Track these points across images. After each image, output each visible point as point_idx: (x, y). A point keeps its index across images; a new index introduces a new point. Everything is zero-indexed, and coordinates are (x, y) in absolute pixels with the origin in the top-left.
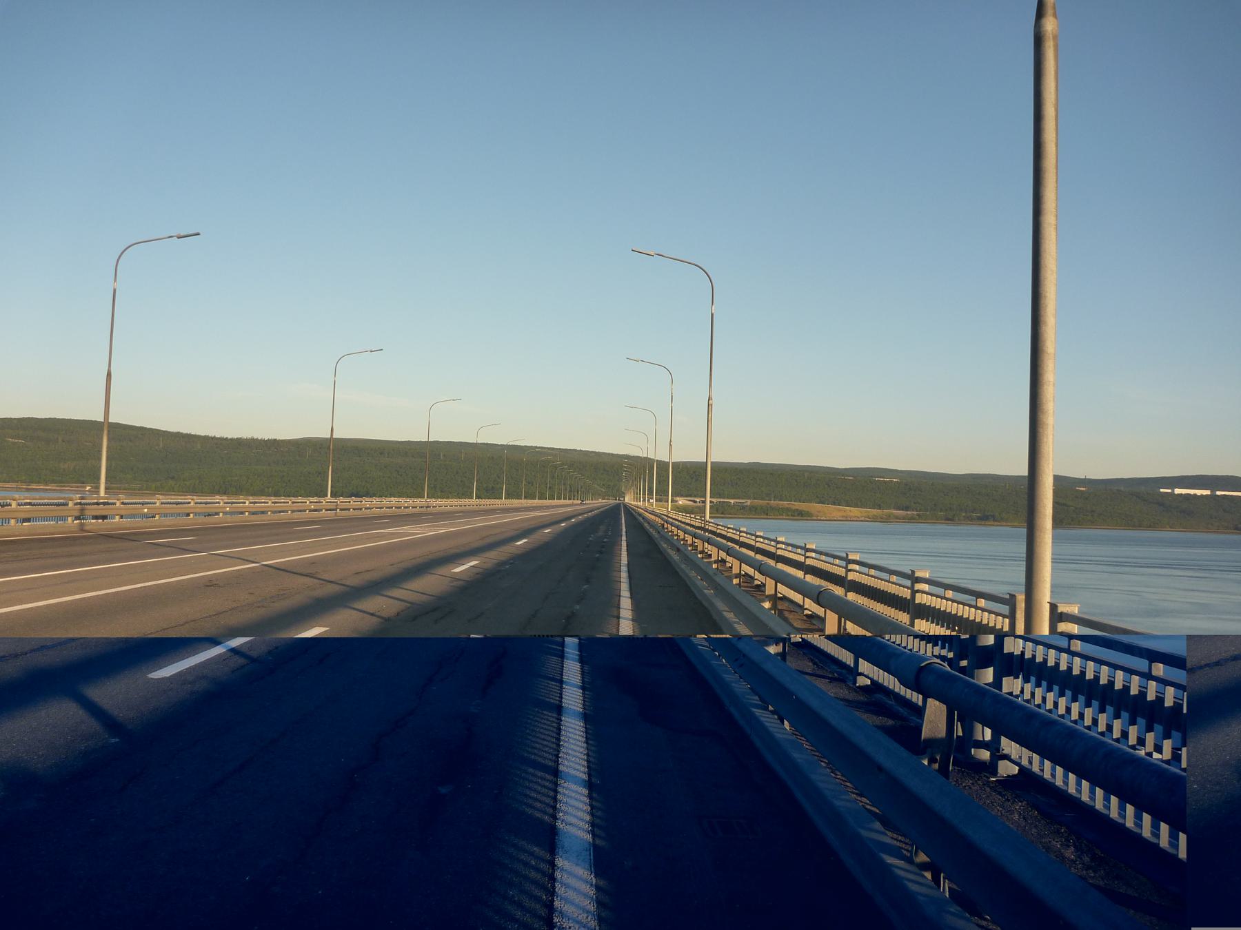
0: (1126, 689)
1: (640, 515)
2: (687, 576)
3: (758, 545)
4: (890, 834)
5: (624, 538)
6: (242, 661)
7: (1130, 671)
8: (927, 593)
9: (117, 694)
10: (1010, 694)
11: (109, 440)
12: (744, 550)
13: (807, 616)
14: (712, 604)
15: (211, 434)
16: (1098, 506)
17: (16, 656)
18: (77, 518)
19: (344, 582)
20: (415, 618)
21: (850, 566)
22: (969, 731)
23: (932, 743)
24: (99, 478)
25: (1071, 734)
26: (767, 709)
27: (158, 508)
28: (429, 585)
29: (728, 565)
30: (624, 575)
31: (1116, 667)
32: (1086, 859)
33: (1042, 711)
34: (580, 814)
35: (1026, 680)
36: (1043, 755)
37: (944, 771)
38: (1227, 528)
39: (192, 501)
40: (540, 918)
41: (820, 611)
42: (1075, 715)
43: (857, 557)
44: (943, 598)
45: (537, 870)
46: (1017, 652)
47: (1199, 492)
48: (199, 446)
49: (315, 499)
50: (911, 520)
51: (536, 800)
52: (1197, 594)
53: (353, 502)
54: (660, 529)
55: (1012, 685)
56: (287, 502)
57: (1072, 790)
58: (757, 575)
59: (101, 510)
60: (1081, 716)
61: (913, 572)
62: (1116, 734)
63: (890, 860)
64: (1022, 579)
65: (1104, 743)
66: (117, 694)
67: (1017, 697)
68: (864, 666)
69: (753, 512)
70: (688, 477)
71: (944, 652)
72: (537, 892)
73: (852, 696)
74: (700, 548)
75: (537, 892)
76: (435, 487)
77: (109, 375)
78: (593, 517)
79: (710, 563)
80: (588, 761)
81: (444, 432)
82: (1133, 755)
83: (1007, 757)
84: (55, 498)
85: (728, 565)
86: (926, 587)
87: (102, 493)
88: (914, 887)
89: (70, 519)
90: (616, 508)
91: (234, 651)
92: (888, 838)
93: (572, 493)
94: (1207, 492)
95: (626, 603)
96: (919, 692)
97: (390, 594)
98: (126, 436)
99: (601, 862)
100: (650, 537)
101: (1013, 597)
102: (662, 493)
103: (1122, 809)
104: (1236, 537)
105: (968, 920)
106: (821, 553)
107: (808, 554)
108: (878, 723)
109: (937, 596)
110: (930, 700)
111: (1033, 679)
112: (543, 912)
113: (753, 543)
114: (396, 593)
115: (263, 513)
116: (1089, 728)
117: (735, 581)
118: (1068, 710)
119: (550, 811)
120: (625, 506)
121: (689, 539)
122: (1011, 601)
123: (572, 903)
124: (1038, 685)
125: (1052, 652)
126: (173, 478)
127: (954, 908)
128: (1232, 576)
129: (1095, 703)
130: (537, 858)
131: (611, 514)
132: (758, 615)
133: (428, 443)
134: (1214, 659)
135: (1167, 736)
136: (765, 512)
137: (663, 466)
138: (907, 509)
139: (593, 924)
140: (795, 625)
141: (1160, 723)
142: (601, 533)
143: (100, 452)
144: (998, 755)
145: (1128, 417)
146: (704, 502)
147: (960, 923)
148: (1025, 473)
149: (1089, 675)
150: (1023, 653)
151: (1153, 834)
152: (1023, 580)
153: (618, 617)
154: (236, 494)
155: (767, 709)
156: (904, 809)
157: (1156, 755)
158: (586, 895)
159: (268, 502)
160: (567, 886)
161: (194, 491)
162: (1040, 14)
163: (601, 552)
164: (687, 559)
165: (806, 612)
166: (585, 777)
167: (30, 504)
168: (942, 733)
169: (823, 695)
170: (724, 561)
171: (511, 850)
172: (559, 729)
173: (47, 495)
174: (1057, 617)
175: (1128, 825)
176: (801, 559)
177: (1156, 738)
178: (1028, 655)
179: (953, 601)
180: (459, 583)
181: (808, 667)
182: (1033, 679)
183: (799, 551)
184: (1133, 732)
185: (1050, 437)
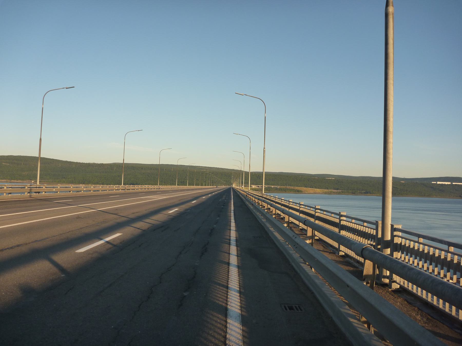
0: (440, 256)
1: (238, 192)
2: (256, 214)
3: (282, 203)
4: (351, 310)
5: (232, 200)
6: (110, 246)
7: (441, 250)
8: (345, 221)
9: (64, 258)
10: (397, 258)
11: (40, 164)
12: (277, 205)
13: (300, 229)
14: (265, 225)
15: (79, 162)
16: (409, 188)
17: (26, 244)
18: (29, 193)
19: (128, 217)
20: (154, 230)
21: (317, 211)
22: (381, 272)
23: (367, 276)
24: (37, 178)
25: (419, 273)
26: (306, 264)
27: (59, 189)
28: (160, 218)
29: (271, 210)
30: (232, 214)
31: (436, 248)
32: (425, 320)
33: (408, 264)
34: (236, 303)
35: (402, 253)
36: (409, 281)
37: (372, 287)
38: (457, 196)
39: (72, 186)
40: (222, 341)
41: (305, 227)
42: (420, 266)
43: (319, 207)
44: (351, 222)
45: (220, 323)
46: (399, 243)
47: (446, 183)
48: (74, 166)
49: (117, 186)
50: (339, 193)
51: (220, 297)
52: (446, 221)
53: (131, 187)
54: (246, 197)
55: (397, 255)
56: (107, 187)
57: (419, 294)
58: (282, 214)
59: (38, 190)
60: (423, 266)
61: (340, 213)
62: (436, 273)
63: (352, 320)
64: (381, 215)
65: (431, 276)
66: (64, 258)
67: (399, 259)
68: (342, 248)
69: (281, 191)
70: (256, 177)
71: (372, 243)
72: (220, 332)
73: (338, 259)
74: (261, 204)
75: (220, 332)
76: (162, 181)
77: (41, 139)
78: (221, 192)
79: (264, 210)
80: (239, 283)
81: (165, 161)
82: (442, 281)
83: (395, 282)
84: (20, 185)
85: (271, 210)
86: (345, 218)
87: (38, 184)
88: (360, 330)
89: (26, 193)
90: (229, 189)
91: (107, 242)
92: (351, 312)
93: (213, 183)
94: (449, 183)
95: (233, 224)
96: (363, 257)
97: (145, 221)
98: (47, 162)
99: (244, 321)
100: (242, 200)
101: (377, 222)
102: (246, 183)
103: (438, 301)
104: (460, 200)
105: (381, 342)
106: (306, 206)
107: (301, 206)
108: (347, 269)
109: (349, 222)
110: (366, 261)
111: (405, 253)
112: (223, 339)
113: (280, 202)
114: (148, 220)
115: (98, 191)
116: (426, 271)
117: (274, 216)
118: (418, 264)
119: (225, 302)
120: (233, 188)
121: (257, 200)
122: (376, 224)
123: (233, 336)
124: (407, 255)
125: (412, 243)
126: (64, 178)
127: (376, 338)
128: (459, 214)
129: (428, 262)
130: (220, 319)
131: (228, 191)
132: (282, 229)
133: (159, 165)
134: (10, 246)
135: (455, 274)
136: (285, 191)
137: (247, 173)
138: (338, 189)
139: (241, 344)
140: (296, 232)
141: (452, 269)
142: (224, 198)
143: (37, 168)
144: (392, 281)
145: (420, 155)
146: (262, 187)
147: (377, 343)
148: (382, 176)
149: (426, 251)
150: (401, 243)
151: (450, 310)
152: (381, 216)
153: (230, 230)
154: (88, 184)
155: (306, 264)
156: (357, 301)
157: (451, 281)
158: (238, 333)
159: (100, 187)
160: (231, 330)
161: (72, 183)
162: (387, 5)
163: (224, 206)
164: (256, 208)
165: (300, 228)
166: (238, 289)
167: (11, 187)
168: (371, 273)
169: (327, 259)
170: (269, 209)
171: (211, 316)
172: (229, 271)
173: (17, 184)
174: (393, 229)
175: (440, 307)
176: (298, 208)
177: (451, 275)
178: (403, 244)
179: (355, 224)
180: (171, 217)
181: (321, 248)
182: (405, 253)
183: (297, 205)
184: (442, 272)
185: (391, 163)
